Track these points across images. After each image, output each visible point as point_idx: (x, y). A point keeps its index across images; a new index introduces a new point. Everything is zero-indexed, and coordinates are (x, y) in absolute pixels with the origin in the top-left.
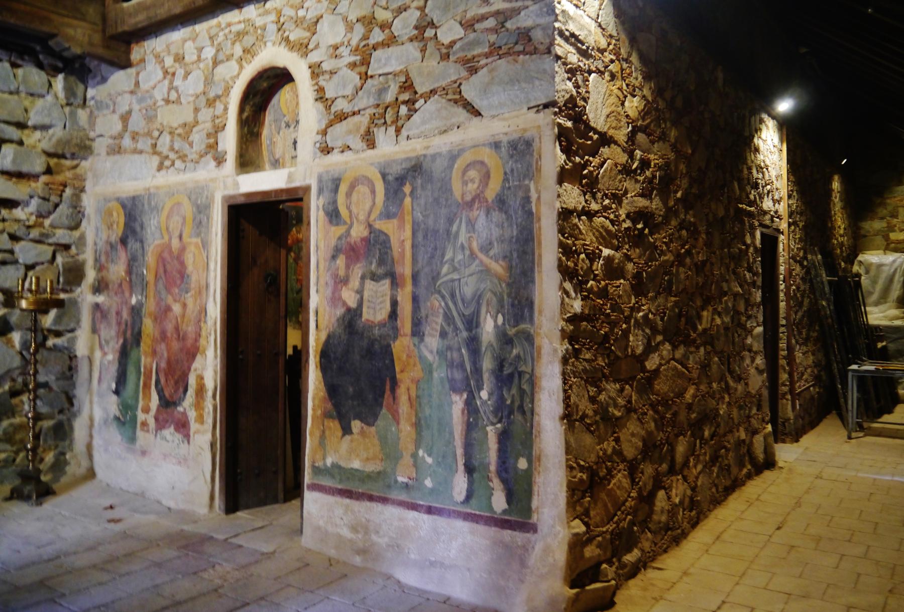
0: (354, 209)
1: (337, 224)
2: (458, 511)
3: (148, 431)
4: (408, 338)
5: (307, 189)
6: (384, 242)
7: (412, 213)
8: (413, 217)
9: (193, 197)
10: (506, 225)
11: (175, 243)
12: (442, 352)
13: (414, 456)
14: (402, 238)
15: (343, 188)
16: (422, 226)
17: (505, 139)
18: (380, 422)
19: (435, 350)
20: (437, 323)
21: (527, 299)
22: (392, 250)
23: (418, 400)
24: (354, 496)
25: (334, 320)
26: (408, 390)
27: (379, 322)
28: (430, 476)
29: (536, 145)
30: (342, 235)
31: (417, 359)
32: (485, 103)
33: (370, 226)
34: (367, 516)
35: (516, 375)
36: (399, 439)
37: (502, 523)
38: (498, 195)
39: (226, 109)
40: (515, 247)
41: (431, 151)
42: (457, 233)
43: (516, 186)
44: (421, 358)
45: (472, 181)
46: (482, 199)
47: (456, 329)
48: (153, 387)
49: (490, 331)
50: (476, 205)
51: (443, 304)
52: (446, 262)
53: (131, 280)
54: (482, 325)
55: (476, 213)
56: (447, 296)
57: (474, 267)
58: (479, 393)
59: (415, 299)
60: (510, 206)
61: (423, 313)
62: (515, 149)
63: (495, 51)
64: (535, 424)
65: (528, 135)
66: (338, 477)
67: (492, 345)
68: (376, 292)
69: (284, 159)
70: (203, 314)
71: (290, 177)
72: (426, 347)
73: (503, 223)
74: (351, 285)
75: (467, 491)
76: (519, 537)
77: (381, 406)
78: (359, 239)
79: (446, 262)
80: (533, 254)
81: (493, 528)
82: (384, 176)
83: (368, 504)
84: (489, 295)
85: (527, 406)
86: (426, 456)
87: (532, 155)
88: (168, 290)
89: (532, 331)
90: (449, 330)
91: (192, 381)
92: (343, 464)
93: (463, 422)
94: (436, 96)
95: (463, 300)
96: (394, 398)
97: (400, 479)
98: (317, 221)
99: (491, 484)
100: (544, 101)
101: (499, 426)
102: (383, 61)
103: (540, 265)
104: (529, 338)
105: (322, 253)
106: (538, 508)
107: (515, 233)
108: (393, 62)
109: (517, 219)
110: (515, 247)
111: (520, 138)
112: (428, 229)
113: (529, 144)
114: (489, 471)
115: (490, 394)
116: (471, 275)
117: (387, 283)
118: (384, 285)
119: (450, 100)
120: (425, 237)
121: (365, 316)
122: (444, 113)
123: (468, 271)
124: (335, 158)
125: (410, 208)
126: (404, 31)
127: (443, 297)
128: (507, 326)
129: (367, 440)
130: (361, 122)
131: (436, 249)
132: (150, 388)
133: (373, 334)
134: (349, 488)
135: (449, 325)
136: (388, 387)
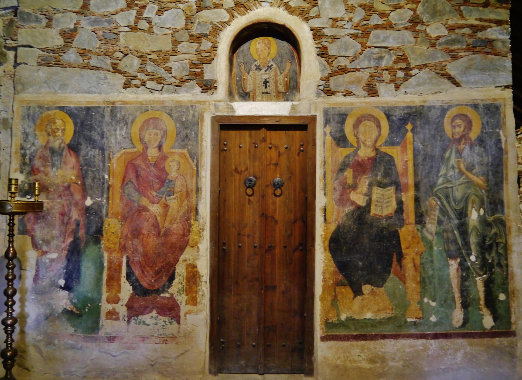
0: (361, 137)
1: (345, 147)
2: (457, 333)
3: (117, 319)
4: (413, 226)
5: (313, 119)
6: (389, 161)
7: (413, 144)
8: (414, 146)
9: (176, 115)
10: (484, 155)
11: (153, 153)
12: (440, 233)
13: (421, 303)
14: (406, 159)
15: (349, 122)
16: (422, 152)
17: (481, 103)
18: (389, 284)
19: (434, 232)
20: (434, 215)
21: (499, 200)
22: (396, 167)
23: (422, 266)
24: (368, 338)
25: (342, 215)
26: (413, 259)
27: (386, 216)
28: (434, 314)
29: (502, 109)
30: (350, 154)
31: (420, 239)
32: (465, 79)
33: (376, 150)
34: (382, 350)
35: (495, 245)
36: (406, 293)
37: (491, 334)
38: (478, 137)
39: (215, 47)
40: (490, 168)
41: (427, 104)
42: (449, 158)
43: (491, 132)
44: (424, 238)
45: (459, 126)
46: (467, 139)
47: (450, 218)
48: (123, 279)
49: (475, 219)
50: (463, 142)
51: (439, 203)
52: (441, 176)
53: (84, 184)
54: (469, 215)
55: (462, 146)
56: (443, 199)
57: (462, 180)
58: (469, 258)
59: (417, 200)
60: (487, 144)
61: (423, 209)
62: (489, 110)
63: (471, 49)
64: (509, 272)
65: (497, 102)
66: (353, 328)
67: (476, 228)
68: (383, 195)
69: (254, 93)
70: (193, 214)
71: (293, 108)
72: (427, 230)
73: (482, 154)
74: (359, 190)
75: (464, 319)
76: (505, 341)
77: (389, 273)
78: (366, 158)
79: (441, 176)
80: (502, 173)
81: (486, 339)
82: (388, 117)
83: (382, 341)
84: (473, 197)
85: (503, 262)
86: (430, 301)
87: (500, 115)
88: (142, 193)
89: (504, 218)
90: (444, 219)
91: (180, 269)
92: (356, 317)
93: (458, 277)
94: (427, 69)
95: (454, 200)
96: (401, 267)
97: (409, 320)
98: (324, 143)
99: (481, 312)
100: (505, 84)
101: (485, 276)
102: (382, 38)
103: (507, 179)
104: (502, 223)
105: (329, 168)
106: (515, 321)
107: (490, 160)
108: (391, 40)
109: (491, 151)
110: (490, 168)
111: (492, 104)
112: (426, 154)
113: (497, 108)
114: (480, 305)
115: (476, 258)
116: (460, 185)
117: (392, 189)
118: (389, 190)
119: (438, 73)
120: (424, 159)
121: (374, 211)
122: (434, 81)
123: (458, 183)
124: (339, 99)
125: (412, 140)
126: (400, 22)
127: (439, 198)
128: (487, 216)
129: (377, 298)
130: (362, 77)
131: (432, 167)
132: (119, 280)
133: (381, 224)
134: (363, 333)
135: (444, 216)
136: (395, 259)
